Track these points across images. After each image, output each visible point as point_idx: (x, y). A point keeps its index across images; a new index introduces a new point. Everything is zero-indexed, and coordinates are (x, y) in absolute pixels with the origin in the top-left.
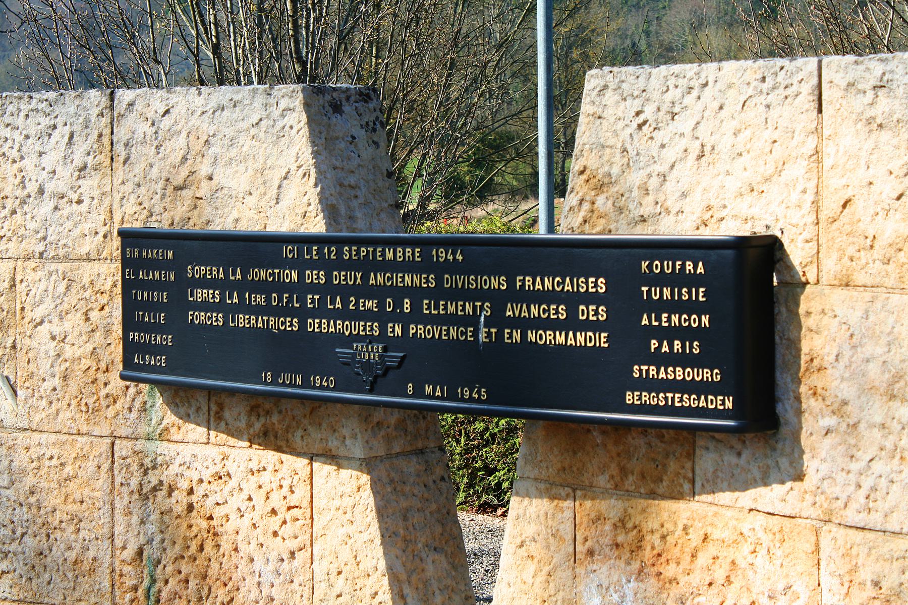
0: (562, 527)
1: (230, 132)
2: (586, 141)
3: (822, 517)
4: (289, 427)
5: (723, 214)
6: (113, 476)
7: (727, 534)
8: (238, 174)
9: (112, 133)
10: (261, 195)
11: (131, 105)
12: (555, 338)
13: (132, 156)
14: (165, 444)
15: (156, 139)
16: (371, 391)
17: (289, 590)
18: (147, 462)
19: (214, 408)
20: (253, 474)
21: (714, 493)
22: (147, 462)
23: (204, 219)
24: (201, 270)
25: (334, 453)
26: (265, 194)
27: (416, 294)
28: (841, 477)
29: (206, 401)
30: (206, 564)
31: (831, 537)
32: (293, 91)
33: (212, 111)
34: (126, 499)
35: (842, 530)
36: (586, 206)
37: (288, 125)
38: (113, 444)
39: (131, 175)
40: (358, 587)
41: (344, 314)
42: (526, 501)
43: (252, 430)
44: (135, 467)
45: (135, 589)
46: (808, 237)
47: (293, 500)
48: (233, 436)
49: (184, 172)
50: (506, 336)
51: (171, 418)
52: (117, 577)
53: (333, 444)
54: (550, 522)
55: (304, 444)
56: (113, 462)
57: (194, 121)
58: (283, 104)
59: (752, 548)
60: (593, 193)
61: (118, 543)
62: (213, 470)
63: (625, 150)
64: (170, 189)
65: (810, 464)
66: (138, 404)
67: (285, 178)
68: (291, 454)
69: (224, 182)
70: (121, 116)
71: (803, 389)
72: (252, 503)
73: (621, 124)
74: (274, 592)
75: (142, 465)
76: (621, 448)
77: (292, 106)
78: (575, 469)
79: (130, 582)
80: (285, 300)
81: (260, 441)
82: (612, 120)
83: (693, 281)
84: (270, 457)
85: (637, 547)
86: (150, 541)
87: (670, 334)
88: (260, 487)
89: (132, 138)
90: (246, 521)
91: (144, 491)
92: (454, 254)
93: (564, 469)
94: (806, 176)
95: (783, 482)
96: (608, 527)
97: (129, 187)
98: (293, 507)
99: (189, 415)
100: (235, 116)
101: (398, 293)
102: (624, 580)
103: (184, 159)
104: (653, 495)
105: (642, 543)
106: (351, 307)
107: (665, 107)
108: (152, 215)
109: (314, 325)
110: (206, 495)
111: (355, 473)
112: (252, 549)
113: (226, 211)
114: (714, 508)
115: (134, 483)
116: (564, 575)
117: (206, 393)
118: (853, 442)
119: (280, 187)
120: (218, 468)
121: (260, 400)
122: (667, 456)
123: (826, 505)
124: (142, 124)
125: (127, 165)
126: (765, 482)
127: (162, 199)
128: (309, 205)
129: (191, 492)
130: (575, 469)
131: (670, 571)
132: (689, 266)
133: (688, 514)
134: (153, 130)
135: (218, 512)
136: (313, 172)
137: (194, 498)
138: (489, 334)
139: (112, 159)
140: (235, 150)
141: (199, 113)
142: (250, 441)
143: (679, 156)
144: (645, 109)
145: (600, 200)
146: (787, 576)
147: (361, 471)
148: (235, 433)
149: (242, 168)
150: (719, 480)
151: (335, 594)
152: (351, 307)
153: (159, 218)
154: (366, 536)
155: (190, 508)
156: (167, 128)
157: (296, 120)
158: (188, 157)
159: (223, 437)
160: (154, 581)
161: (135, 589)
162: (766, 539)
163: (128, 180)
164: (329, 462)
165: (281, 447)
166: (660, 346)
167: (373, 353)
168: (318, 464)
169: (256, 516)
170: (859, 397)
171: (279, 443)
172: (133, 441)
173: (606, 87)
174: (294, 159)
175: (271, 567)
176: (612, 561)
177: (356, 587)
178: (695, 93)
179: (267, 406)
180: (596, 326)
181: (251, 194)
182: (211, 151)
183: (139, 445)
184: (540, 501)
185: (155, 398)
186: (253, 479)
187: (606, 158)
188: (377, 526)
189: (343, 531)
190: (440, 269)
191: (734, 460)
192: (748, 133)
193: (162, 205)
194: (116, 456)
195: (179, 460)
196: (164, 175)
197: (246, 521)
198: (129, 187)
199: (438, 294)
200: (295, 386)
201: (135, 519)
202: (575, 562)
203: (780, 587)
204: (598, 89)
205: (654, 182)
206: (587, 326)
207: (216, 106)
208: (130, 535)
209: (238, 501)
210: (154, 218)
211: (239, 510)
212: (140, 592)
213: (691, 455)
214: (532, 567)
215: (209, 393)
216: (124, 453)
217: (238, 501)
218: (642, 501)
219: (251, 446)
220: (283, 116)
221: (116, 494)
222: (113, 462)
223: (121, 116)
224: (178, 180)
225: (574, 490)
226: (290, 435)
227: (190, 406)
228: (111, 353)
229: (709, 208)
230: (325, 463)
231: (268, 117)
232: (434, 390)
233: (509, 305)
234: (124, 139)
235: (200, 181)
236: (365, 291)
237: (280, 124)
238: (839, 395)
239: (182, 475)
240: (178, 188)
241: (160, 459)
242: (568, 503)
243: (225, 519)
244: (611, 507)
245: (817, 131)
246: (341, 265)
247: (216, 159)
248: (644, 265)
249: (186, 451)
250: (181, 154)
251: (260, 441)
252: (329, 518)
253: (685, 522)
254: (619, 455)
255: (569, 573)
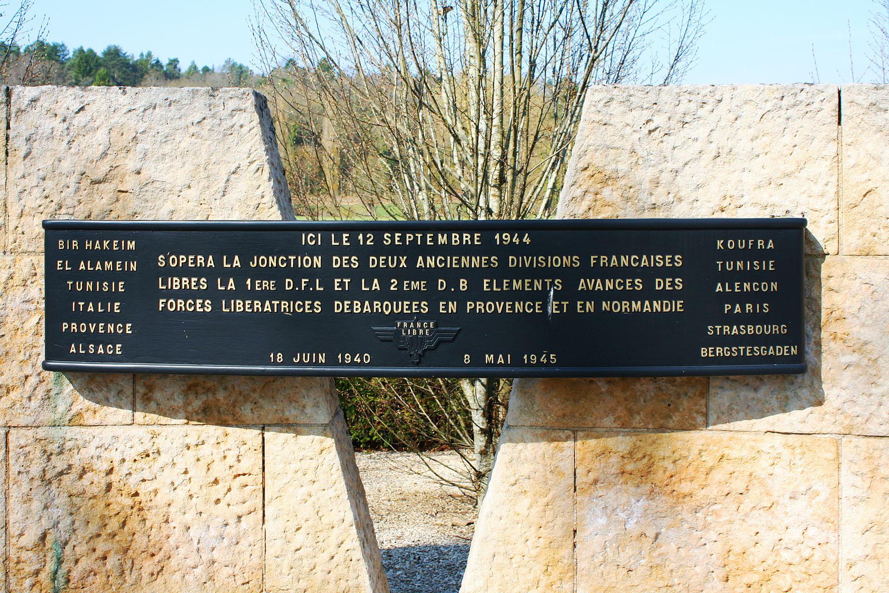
0: (561, 464)
1: (165, 130)
2: (591, 142)
3: (842, 431)
4: (235, 402)
5: (741, 202)
6: (7, 466)
7: (745, 453)
8: (173, 169)
9: (8, 128)
10: (204, 188)
11: (35, 101)
12: (630, 306)
13: (34, 152)
14: (77, 429)
15: (68, 134)
16: (417, 365)
17: (236, 551)
18: (53, 448)
19: (141, 390)
20: (188, 449)
21: (729, 422)
22: (53, 448)
23: (130, 212)
24: (175, 261)
25: (291, 421)
26: (208, 187)
27: (474, 275)
28: (863, 400)
29: (131, 384)
30: (129, 539)
31: (851, 448)
32: (244, 94)
33: (142, 109)
34: (25, 488)
35: (863, 441)
36: (590, 197)
37: (238, 124)
38: (7, 434)
39: (34, 169)
40: (320, 539)
41: (384, 295)
42: (520, 446)
43: (190, 409)
44: (38, 453)
45: (37, 573)
46: (832, 219)
47: (242, 468)
48: (165, 415)
49: (103, 168)
50: (579, 307)
51: (82, 403)
52: (12, 565)
53: (291, 413)
54: (548, 462)
55: (256, 415)
56: (7, 452)
57: (115, 118)
58: (232, 104)
59: (771, 462)
60: (599, 186)
61: (14, 530)
62: (141, 449)
63: (633, 151)
64: (86, 183)
65: (830, 391)
66: (40, 392)
67: (234, 173)
68: (237, 426)
69: (156, 176)
70: (20, 111)
71: (824, 335)
72: (188, 476)
73: (628, 130)
74: (216, 555)
75: (45, 451)
76: (629, 393)
77: (243, 107)
78: (577, 415)
79: (29, 568)
80: (303, 285)
81: (200, 417)
82: (620, 126)
83: (763, 255)
84: (212, 431)
85: (647, 473)
86: (56, 525)
87: (743, 297)
88: (198, 460)
89: (36, 133)
90: (182, 493)
91: (48, 476)
92: (521, 237)
93: (564, 415)
94: (829, 172)
95: (802, 408)
96: (614, 459)
97: (32, 181)
98: (239, 475)
99: (107, 399)
100: (170, 114)
101: (452, 276)
102: (633, 501)
103: (105, 154)
104: (662, 429)
105: (652, 469)
106: (392, 288)
107: (678, 117)
108: (61, 208)
109: (339, 307)
110: (130, 474)
111: (317, 438)
112: (189, 517)
113: (158, 203)
114: (729, 434)
115: (35, 470)
116: (564, 503)
117: (131, 376)
118: (874, 372)
119: (228, 180)
120: (147, 446)
121: (201, 379)
122: (678, 396)
123: (847, 422)
124: (48, 120)
125: (27, 160)
126: (784, 409)
127: (76, 192)
128: (263, 197)
129: (110, 472)
130: (577, 415)
131: (685, 487)
132: (760, 243)
133: (703, 441)
134: (65, 125)
135: (143, 489)
136: (267, 168)
137: (113, 477)
138: (560, 307)
139: (7, 153)
140: (169, 147)
141: (125, 110)
142: (187, 418)
143: (694, 156)
144: (654, 118)
145: (606, 192)
146: (808, 479)
147: (326, 435)
148: (172, 413)
149: (178, 163)
150: (734, 412)
151: (294, 548)
152: (392, 288)
153: (71, 211)
154: (331, 493)
155: (109, 487)
156: (83, 124)
157: (248, 119)
158: (109, 152)
159: (153, 417)
160: (60, 562)
161: (37, 573)
162: (786, 454)
163: (29, 175)
164: (285, 430)
165: (225, 421)
166: (733, 308)
167: (422, 329)
168: (271, 433)
169: (194, 488)
170: (881, 338)
171: (224, 417)
172: (34, 430)
173: (612, 99)
174: (247, 155)
175: (213, 532)
176: (618, 487)
177: (318, 539)
178: (708, 107)
179: (210, 384)
180: (671, 295)
181: (189, 187)
182: (140, 147)
183: (41, 433)
184: (536, 444)
185: (62, 385)
186: (191, 454)
187: (610, 158)
188: (343, 483)
189: (304, 490)
190: (504, 251)
191: (751, 394)
192: (766, 139)
193: (76, 199)
194: (11, 446)
195: (96, 442)
196: (79, 169)
197: (182, 493)
198: (32, 181)
199: (502, 273)
200: (317, 364)
201: (36, 505)
202: (575, 490)
203: (803, 489)
204: (605, 101)
205: (665, 177)
206: (663, 295)
207: (148, 105)
208: (29, 522)
209: (173, 474)
210: (63, 211)
211: (173, 483)
212: (44, 576)
213: (704, 394)
214: (526, 501)
215: (134, 375)
216: (22, 442)
217: (173, 474)
218: (653, 434)
219: (187, 423)
220: (232, 116)
221: (11, 483)
222: (7, 452)
223: (20, 111)
224: (99, 174)
225: (574, 432)
226: (237, 409)
227: (109, 390)
228: (6, 345)
229: (725, 197)
230: (281, 432)
231: (213, 116)
232: (496, 359)
233: (582, 280)
234: (26, 134)
235: (124, 175)
236: (413, 273)
237: (229, 123)
238: (862, 338)
239: (99, 457)
240: (94, 182)
241: (69, 444)
242: (570, 443)
243: (153, 494)
244: (620, 443)
245: (837, 139)
246: (379, 249)
247: (145, 154)
248: (719, 243)
249: (105, 435)
250: (101, 149)
251: (200, 417)
252: (285, 481)
253: (701, 447)
254: (626, 399)
255: (570, 501)
